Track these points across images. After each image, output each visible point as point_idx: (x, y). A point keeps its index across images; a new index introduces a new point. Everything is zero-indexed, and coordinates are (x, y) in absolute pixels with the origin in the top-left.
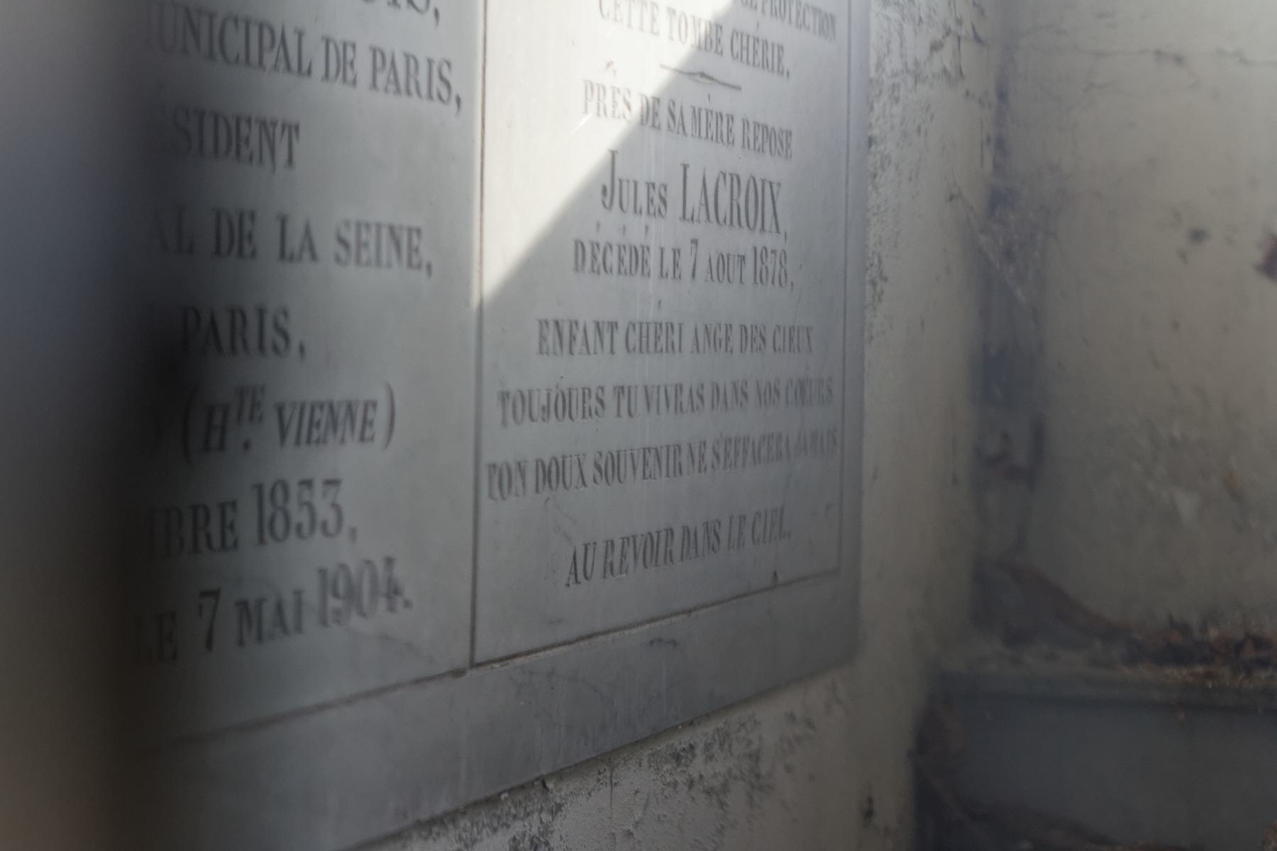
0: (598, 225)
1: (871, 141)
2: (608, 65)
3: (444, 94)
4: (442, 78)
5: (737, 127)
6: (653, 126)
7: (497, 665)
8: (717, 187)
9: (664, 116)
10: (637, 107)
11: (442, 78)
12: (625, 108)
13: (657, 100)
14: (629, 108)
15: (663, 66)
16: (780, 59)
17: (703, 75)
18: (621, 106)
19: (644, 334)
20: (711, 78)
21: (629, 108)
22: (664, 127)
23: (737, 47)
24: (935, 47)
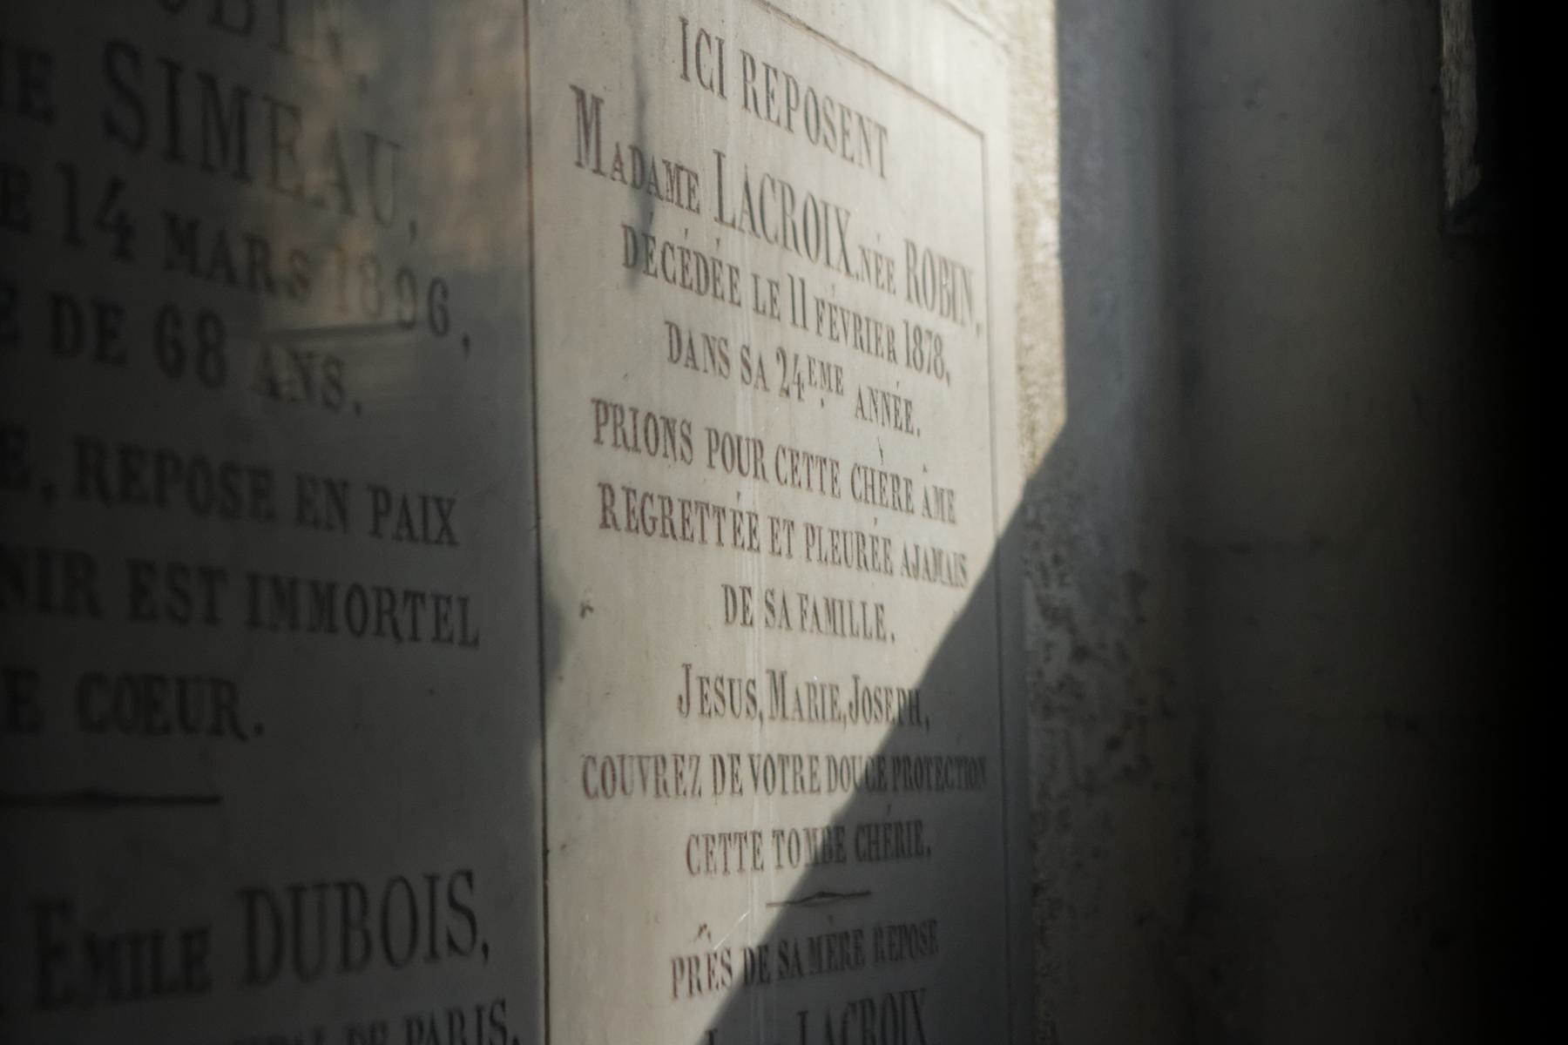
0: (879, 236)
1: (1036, 889)
2: (701, 930)
3: (463, 938)
4: (453, 904)
5: (868, 943)
6: (761, 979)
7: (842, 43)
8: (845, 1023)
9: (774, 962)
10: (738, 964)
11: (453, 904)
12: (725, 972)
13: (764, 948)
14: (730, 970)
15: (770, 905)
16: (917, 836)
17: (822, 894)
18: (720, 971)
19: (899, 1008)
20: (833, 895)
21: (730, 970)
22: (774, 976)
23: (863, 843)
24: (1114, 744)
